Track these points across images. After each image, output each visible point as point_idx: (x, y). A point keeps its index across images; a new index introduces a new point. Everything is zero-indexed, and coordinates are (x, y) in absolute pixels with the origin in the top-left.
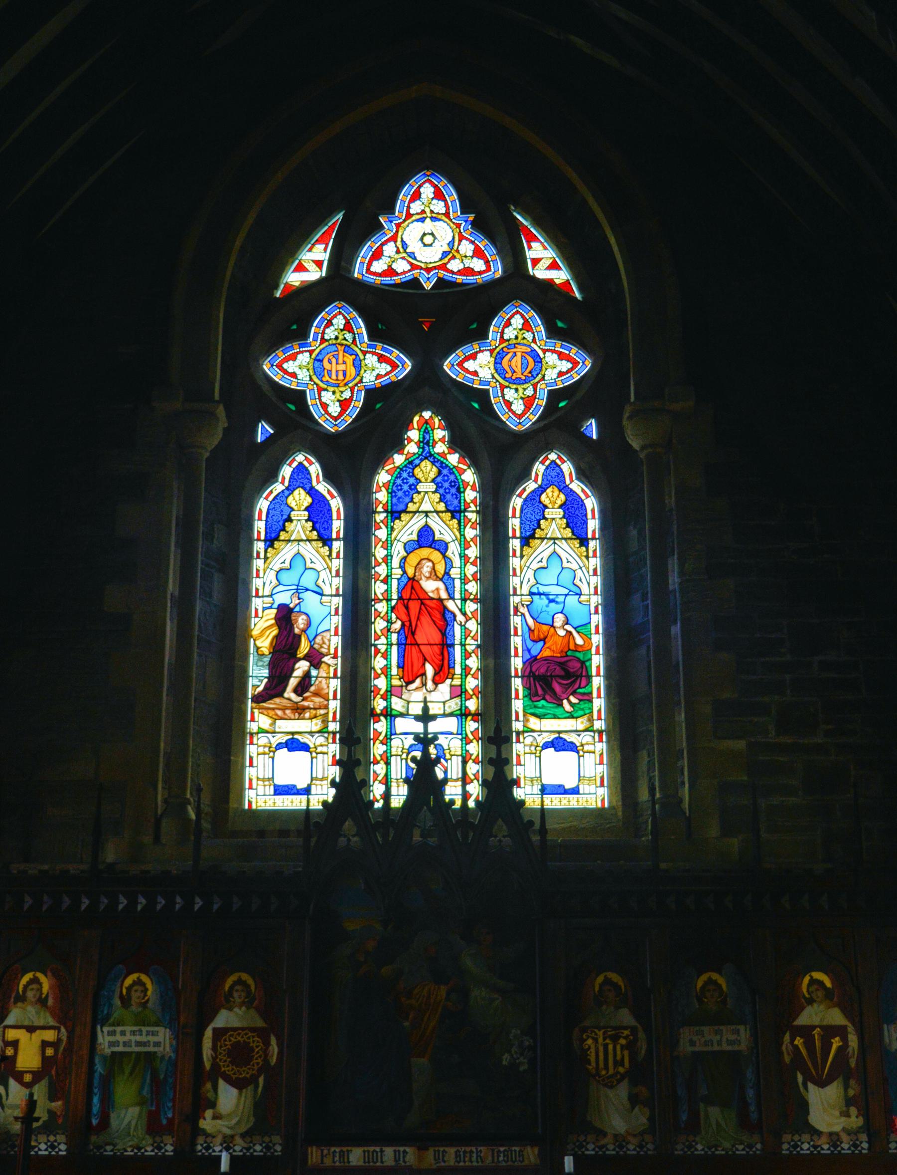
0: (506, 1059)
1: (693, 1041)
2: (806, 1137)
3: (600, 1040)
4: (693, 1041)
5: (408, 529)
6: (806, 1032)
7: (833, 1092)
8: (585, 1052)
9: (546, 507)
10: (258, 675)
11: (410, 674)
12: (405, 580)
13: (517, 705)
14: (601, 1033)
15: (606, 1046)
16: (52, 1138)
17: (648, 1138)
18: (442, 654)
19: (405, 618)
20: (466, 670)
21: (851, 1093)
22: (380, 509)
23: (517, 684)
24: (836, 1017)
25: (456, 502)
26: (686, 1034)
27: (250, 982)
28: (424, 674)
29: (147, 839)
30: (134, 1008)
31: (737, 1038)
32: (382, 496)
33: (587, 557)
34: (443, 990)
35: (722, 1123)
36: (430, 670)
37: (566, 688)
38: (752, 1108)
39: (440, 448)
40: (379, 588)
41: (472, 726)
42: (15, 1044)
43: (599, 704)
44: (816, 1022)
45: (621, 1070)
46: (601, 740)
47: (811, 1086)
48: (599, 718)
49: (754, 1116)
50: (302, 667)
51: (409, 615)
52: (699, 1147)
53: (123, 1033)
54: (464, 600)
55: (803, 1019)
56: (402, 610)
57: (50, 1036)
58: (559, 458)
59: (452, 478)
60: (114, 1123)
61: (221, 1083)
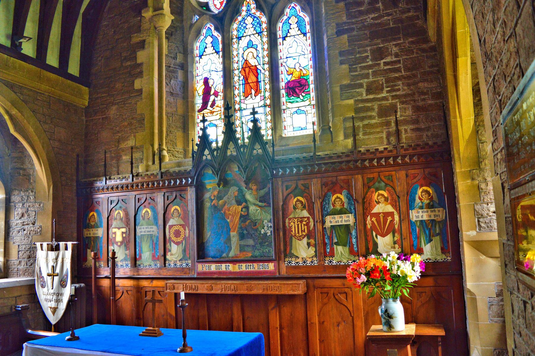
0: (263, 232)
1: (330, 221)
2: (293, 259)
3: (296, 223)
4: (330, 221)
5: (244, 42)
6: (377, 215)
7: (389, 238)
8: (291, 227)
9: (291, 24)
10: (199, 102)
11: (247, 95)
12: (244, 61)
13: (283, 100)
14: (296, 220)
15: (298, 225)
16: (186, 262)
17: (315, 259)
18: (257, 85)
19: (244, 74)
20: (265, 90)
21: (396, 239)
22: (234, 37)
23: (283, 92)
24: (389, 208)
25: (259, 29)
26: (328, 219)
27: (179, 209)
28: (251, 93)
29: (150, 163)
30: (146, 220)
31: (349, 219)
32: (235, 33)
33: (306, 40)
34: (240, 207)
35: (343, 252)
36: (253, 92)
37: (300, 90)
38: (355, 246)
39: (253, 11)
40: (235, 66)
41: (268, 109)
42: (115, 233)
43: (313, 94)
44: (381, 211)
45: (304, 234)
46: (314, 108)
47: (378, 236)
48: (313, 100)
49: (356, 249)
50: (212, 98)
51: (245, 73)
52: (334, 262)
53: (143, 228)
54: (264, 64)
55: (375, 211)
56: (243, 72)
57: (124, 230)
58: (295, 5)
59: (258, 21)
60: (143, 257)
61: (172, 243)
